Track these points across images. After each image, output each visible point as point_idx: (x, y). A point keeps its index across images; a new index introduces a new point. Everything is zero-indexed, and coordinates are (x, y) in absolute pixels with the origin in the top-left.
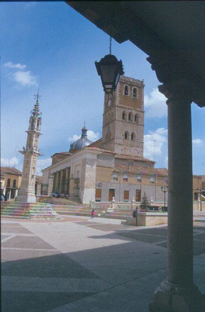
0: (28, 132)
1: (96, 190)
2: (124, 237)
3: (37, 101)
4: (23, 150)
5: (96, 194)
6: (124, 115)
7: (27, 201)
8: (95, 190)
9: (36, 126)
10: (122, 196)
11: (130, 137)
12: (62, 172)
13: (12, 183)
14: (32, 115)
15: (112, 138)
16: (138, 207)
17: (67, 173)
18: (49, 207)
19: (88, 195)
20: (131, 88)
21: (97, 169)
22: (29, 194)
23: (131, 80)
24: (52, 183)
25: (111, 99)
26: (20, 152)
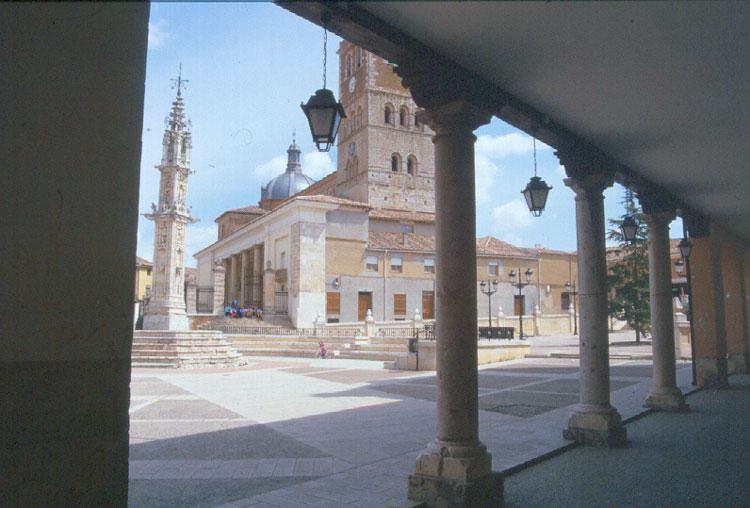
0: (161, 169)
3: (179, 94)
6: (387, 112)
8: (323, 296)
9: (179, 152)
10: (390, 307)
15: (360, 172)
19: (310, 309)
25: (354, 75)
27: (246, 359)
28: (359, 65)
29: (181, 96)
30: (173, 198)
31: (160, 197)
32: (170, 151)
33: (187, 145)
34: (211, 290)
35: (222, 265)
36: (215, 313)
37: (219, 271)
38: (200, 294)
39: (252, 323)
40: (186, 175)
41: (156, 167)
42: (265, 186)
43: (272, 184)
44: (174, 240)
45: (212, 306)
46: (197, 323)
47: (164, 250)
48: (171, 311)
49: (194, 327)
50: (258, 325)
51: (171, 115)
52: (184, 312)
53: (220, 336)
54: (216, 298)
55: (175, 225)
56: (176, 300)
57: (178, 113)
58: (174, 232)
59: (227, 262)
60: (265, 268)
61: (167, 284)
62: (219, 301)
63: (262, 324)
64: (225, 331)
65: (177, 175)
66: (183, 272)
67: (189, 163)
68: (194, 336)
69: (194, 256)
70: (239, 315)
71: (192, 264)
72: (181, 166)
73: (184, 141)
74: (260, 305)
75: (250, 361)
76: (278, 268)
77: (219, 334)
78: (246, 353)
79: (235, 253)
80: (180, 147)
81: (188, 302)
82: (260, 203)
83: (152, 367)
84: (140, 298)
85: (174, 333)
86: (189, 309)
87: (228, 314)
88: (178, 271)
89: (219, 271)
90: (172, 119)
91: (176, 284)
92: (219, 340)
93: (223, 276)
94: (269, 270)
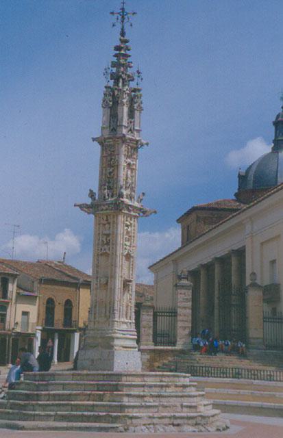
0: (101, 142)
3: (123, 34)
17: (234, 268)
26: (82, 207)
27: (224, 418)
29: (126, 38)
30: (117, 181)
31: (101, 180)
32: (114, 116)
33: (136, 106)
34: (173, 313)
35: (187, 279)
36: (179, 347)
37: (183, 287)
38: (159, 319)
39: (232, 362)
40: (136, 149)
41: (94, 140)
42: (243, 172)
43: (254, 168)
44: (120, 240)
45: (175, 337)
46: (154, 361)
47: (106, 255)
48: (116, 342)
49: (150, 366)
50: (241, 366)
51: (114, 65)
52: (134, 344)
53: (187, 381)
54: (179, 324)
55: (121, 218)
56: (124, 327)
57: (122, 61)
58: (121, 229)
59: (194, 274)
60: (248, 282)
61: (112, 304)
62: (185, 328)
63: (245, 364)
64: (193, 371)
65: (124, 148)
66: (133, 287)
67: (138, 131)
68: (150, 381)
69: (149, 268)
70: (212, 350)
71: (148, 279)
72: (129, 136)
73: (132, 101)
74: (242, 335)
75: (233, 422)
76: (267, 282)
77: (186, 379)
78: (225, 408)
79: (193, 268)
80: (126, 109)
81: (142, 330)
82: (236, 195)
83: (87, 429)
84: (81, 325)
85: (119, 375)
86: (143, 338)
87: (196, 348)
88: (126, 284)
89: (183, 287)
90: (114, 70)
91: (125, 302)
92: (184, 386)
93: (189, 294)
94: (254, 285)
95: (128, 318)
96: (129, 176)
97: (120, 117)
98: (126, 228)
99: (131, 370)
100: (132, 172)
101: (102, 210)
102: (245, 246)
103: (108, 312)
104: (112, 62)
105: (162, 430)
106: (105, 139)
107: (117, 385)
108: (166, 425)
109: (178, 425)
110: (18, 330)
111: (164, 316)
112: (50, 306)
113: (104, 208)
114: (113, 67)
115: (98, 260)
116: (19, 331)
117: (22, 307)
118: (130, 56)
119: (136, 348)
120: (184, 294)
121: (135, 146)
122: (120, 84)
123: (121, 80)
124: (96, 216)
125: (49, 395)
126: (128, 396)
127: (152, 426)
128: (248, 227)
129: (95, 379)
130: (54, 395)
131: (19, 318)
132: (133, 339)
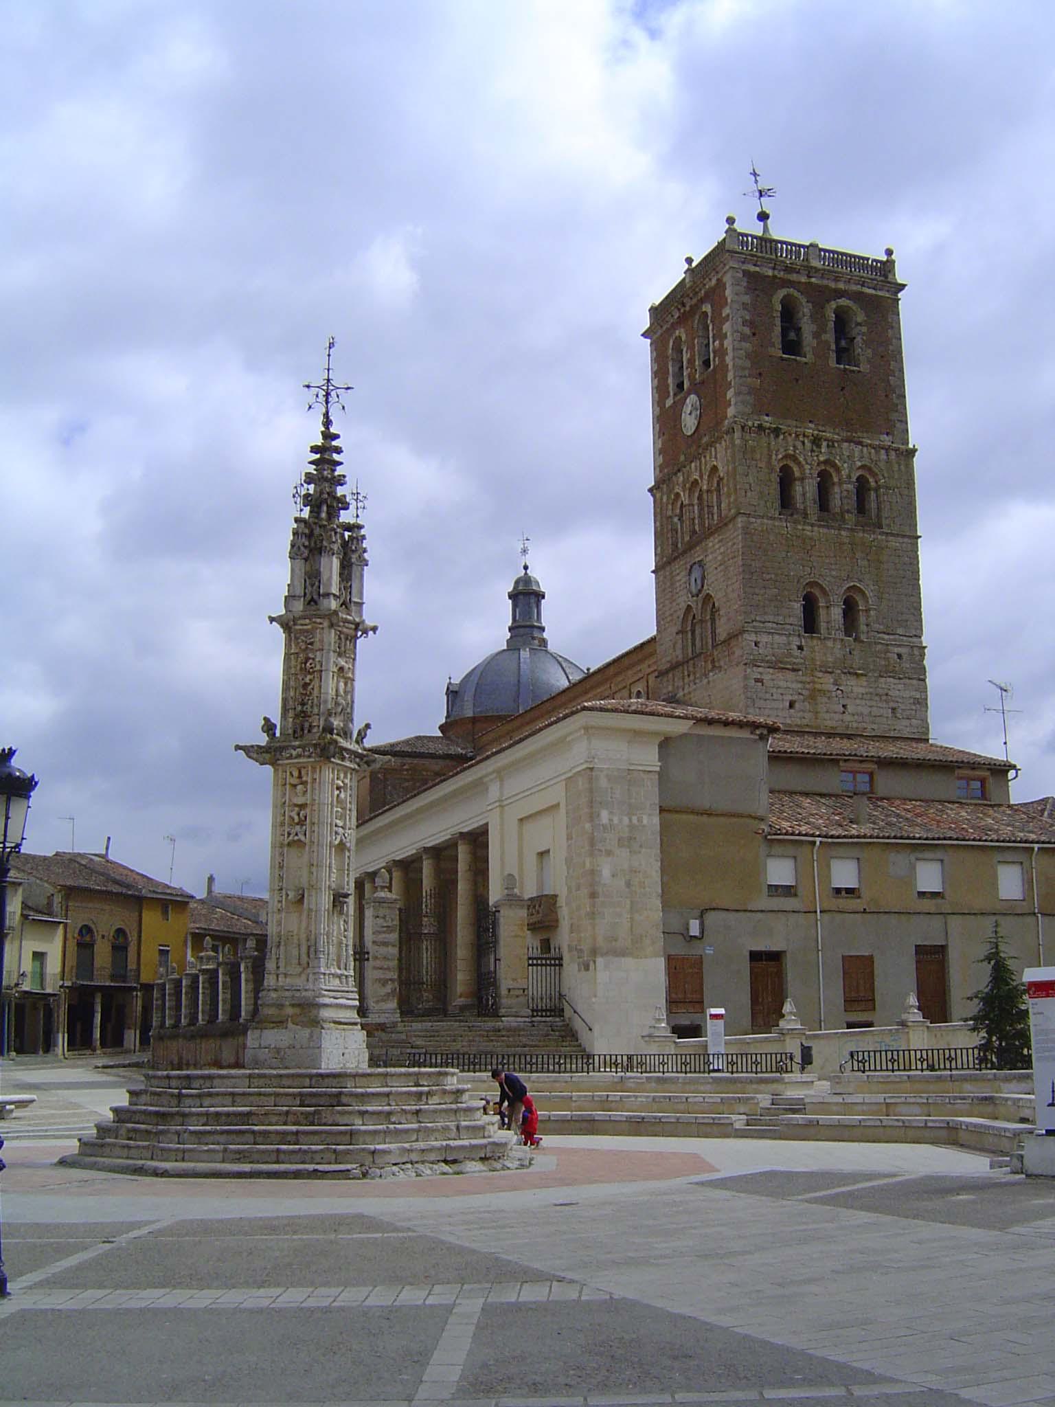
0: (286, 624)
1: (670, 959)
2: (276, 1223)
3: (327, 423)
4: (263, 740)
5: (671, 989)
6: (786, 481)
7: (316, 1062)
8: (661, 963)
9: (336, 578)
10: (831, 992)
11: (837, 613)
12: (427, 868)
13: (102, 954)
14: (306, 514)
15: (722, 633)
16: (796, 1067)
17: (462, 866)
18: (459, 1092)
19: (621, 1000)
20: (819, 307)
21: (664, 827)
22: (325, 1014)
23: (815, 263)
24: (394, 937)
25: (696, 388)
26: (248, 750)
28: (707, 363)
29: (333, 430)
33: (354, 557)
47: (299, 844)
51: (309, 479)
52: (353, 1016)
62: (384, 982)
74: (484, 997)
76: (530, 892)
95: (342, 966)
96: (342, 692)
97: (324, 577)
98: (336, 792)
99: (351, 1067)
100: (346, 684)
101: (291, 757)
102: (487, 824)
103: (304, 956)
104: (307, 474)
105: (429, 1172)
106: (295, 620)
107: (340, 1093)
108: (432, 1163)
109: (455, 1162)
110: (26, 987)
111: (546, 965)
112: (84, 942)
113: (294, 753)
114: (309, 483)
115: (282, 854)
116: (27, 989)
117: (31, 945)
118: (341, 463)
119: (356, 1024)
120: (384, 917)
121: (352, 632)
122: (324, 515)
123: (325, 508)
124: (276, 771)
125: (207, 1114)
126: (362, 1113)
127: (409, 1166)
128: (494, 791)
129: (295, 1084)
130: (218, 1114)
131: (28, 965)
132: (354, 1007)
